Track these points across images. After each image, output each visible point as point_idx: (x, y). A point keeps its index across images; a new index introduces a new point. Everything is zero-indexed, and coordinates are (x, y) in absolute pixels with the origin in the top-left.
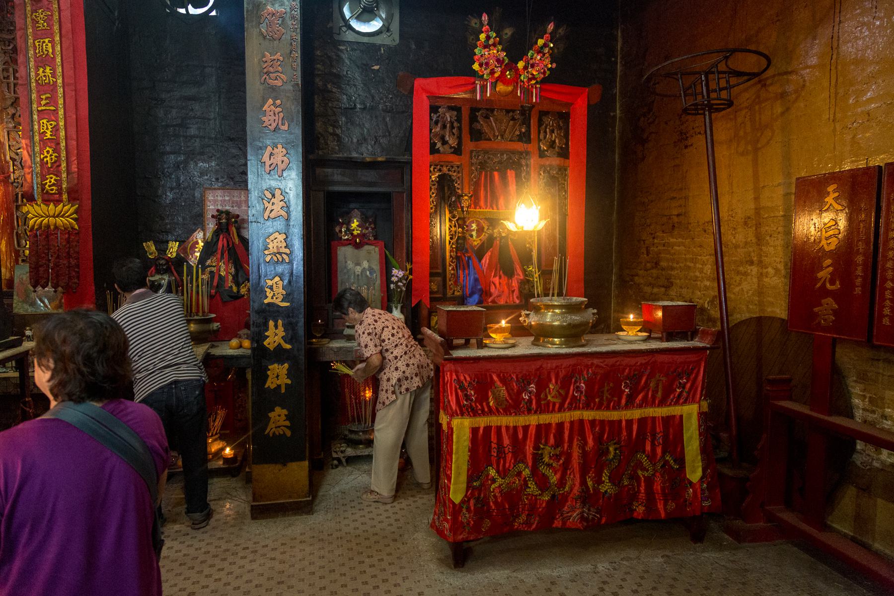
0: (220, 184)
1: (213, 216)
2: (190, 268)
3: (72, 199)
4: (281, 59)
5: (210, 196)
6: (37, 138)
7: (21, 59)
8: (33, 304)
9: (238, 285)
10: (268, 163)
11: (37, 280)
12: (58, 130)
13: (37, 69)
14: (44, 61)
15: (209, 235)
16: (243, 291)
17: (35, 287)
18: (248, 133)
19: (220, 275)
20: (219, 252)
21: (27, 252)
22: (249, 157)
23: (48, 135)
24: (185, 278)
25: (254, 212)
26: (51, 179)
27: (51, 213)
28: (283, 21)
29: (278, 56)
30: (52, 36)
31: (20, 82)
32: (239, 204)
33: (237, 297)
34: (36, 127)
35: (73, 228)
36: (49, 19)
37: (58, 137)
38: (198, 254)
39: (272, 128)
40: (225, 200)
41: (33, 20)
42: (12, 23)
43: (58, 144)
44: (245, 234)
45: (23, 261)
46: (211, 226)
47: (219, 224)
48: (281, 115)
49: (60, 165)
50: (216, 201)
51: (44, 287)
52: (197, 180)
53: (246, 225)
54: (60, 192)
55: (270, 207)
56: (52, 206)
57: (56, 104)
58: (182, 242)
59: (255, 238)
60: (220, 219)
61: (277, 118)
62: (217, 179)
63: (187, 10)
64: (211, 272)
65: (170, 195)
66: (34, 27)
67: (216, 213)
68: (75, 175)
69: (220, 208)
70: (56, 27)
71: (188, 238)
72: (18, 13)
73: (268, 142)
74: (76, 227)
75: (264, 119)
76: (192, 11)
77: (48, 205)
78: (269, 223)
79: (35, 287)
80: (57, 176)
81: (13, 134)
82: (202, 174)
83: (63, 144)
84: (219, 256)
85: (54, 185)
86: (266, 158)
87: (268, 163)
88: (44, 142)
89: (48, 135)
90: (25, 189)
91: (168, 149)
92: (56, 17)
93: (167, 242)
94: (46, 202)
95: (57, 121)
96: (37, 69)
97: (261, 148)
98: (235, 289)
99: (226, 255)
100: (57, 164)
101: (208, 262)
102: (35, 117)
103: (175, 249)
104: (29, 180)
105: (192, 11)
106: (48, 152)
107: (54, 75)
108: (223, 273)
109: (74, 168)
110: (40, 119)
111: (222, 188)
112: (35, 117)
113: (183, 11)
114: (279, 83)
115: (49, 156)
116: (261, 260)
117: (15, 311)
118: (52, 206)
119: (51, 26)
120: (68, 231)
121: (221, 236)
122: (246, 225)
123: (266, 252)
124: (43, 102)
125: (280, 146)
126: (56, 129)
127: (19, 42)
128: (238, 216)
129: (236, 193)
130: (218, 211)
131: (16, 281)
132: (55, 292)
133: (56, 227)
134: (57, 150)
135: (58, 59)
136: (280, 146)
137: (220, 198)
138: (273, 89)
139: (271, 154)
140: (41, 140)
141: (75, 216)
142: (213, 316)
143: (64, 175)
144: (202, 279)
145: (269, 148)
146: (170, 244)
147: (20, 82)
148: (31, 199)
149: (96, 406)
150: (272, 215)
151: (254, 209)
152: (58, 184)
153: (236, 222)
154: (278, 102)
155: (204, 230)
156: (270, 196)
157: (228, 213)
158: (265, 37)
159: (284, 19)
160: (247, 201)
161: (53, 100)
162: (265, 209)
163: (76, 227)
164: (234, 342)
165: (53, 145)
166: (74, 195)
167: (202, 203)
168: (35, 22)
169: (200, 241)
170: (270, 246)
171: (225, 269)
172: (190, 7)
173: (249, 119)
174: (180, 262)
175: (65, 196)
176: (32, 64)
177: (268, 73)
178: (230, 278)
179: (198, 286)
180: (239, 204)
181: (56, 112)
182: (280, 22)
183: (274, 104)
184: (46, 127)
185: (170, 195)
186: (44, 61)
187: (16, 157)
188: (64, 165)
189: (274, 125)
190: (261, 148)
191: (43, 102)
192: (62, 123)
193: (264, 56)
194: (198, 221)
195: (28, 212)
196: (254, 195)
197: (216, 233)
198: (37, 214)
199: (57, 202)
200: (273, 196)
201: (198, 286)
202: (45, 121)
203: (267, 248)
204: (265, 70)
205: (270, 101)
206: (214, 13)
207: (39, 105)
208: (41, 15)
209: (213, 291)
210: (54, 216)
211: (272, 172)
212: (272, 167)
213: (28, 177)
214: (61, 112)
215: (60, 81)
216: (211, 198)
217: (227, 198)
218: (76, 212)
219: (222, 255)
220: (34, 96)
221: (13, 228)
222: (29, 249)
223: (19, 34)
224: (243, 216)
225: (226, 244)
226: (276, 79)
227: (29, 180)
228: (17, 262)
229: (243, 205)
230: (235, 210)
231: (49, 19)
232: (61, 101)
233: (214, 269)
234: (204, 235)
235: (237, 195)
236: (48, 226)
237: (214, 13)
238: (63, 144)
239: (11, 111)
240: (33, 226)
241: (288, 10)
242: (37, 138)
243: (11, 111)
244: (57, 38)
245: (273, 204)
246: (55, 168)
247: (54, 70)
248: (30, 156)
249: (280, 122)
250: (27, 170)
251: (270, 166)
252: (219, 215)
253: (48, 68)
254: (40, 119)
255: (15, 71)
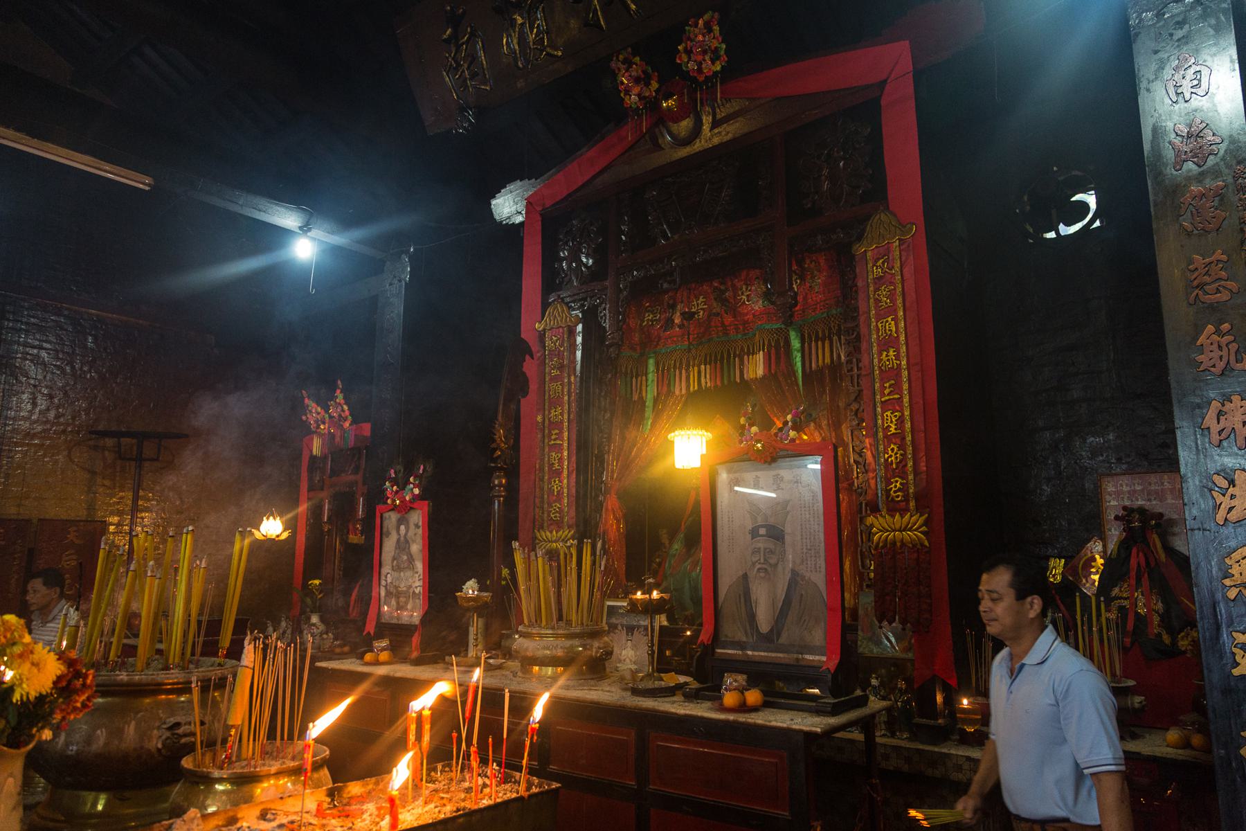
0: (1124, 467)
1: (1117, 518)
2: (1084, 597)
3: (919, 509)
4: (1224, 257)
5: (1109, 486)
6: (881, 434)
7: (864, 346)
8: (879, 643)
9: (1173, 633)
10: (1215, 428)
11: (884, 614)
12: (903, 422)
13: (880, 354)
14: (889, 342)
15: (1112, 546)
16: (1183, 644)
17: (880, 622)
18: (1173, 384)
19: (1137, 614)
20: (1133, 574)
21: (872, 575)
22: (1177, 423)
23: (893, 430)
24: (1078, 617)
25: (1195, 512)
26: (897, 483)
27: (897, 527)
28: (1222, 200)
29: (1219, 255)
30: (895, 312)
31: (863, 373)
32: (1160, 496)
33: (1172, 652)
34: (880, 422)
35: (922, 545)
36: (892, 296)
37: (903, 431)
38: (1096, 577)
39: (1217, 370)
40: (1135, 491)
41: (876, 300)
42: (856, 309)
43: (904, 438)
44: (1179, 545)
45: (868, 586)
46: (1115, 533)
47: (1129, 530)
48: (1234, 347)
49: (906, 465)
50: (1119, 493)
51: (890, 623)
52: (1087, 463)
53: (1176, 530)
54: (906, 499)
55: (1226, 502)
56: (897, 516)
57: (901, 394)
58: (1068, 559)
59: (1201, 556)
60: (1129, 522)
61: (1224, 353)
62: (1119, 460)
63: (1057, 233)
64: (1122, 609)
65: (1047, 489)
66: (877, 307)
67: (1121, 513)
68: (924, 476)
69: (1127, 503)
70: (899, 301)
71: (1079, 552)
72: (861, 296)
73: (1212, 394)
74: (926, 543)
75: (1200, 358)
76: (1066, 230)
77: (893, 516)
78: (1230, 530)
79: (880, 622)
80: (902, 478)
81: (856, 433)
82: (1095, 453)
83: (909, 438)
84: (1133, 582)
85: (899, 490)
86: (1210, 419)
87: (1215, 428)
88: (888, 439)
89: (893, 430)
90: (869, 497)
91: (1041, 423)
92: (899, 289)
93: (1047, 558)
94: (892, 511)
95: (902, 411)
96: (880, 354)
97: (1199, 406)
98: (1166, 639)
99: (1145, 580)
100: (902, 463)
101: (1116, 591)
102: (879, 409)
103: (1059, 570)
104: (873, 486)
105: (1066, 230)
106: (893, 450)
107: (898, 357)
108: (1142, 611)
109: (923, 466)
110: (884, 411)
111: (1129, 472)
112: (879, 409)
113: (1052, 235)
114: (1224, 296)
115: (892, 454)
116: (1219, 596)
117: (860, 650)
118: (897, 516)
119: (893, 301)
120: (916, 547)
121: (1134, 551)
122: (1176, 530)
123: (1227, 582)
124: (886, 392)
125: (1236, 398)
126: (901, 421)
127: (863, 330)
128: (1161, 515)
129: (1153, 478)
130: (1125, 508)
131: (861, 612)
132: (904, 629)
133: (903, 544)
134: (902, 447)
135: (902, 338)
136: (1236, 398)
137: (1125, 489)
138: (1213, 308)
139: (1220, 414)
140: (886, 436)
141: (924, 528)
142: (1131, 683)
143: (911, 477)
144: (1107, 619)
145: (1215, 405)
146: (1052, 563)
147: (863, 373)
148: (875, 509)
149: (843, 426)
150: (1233, 516)
151: (1197, 505)
152: (904, 489)
153: (1158, 525)
154: (1226, 326)
155: (1103, 539)
156: (1225, 484)
157: (1142, 511)
158: (1189, 234)
159: (1222, 198)
160: (1180, 493)
161: (897, 388)
162: (1217, 507)
163: (926, 543)
164: (1173, 735)
165: (898, 441)
166: (923, 502)
167: (1097, 498)
168: (877, 301)
169: (1097, 557)
170: (1235, 571)
171: (1144, 603)
172: (1062, 227)
173: (1171, 363)
174: (1070, 588)
175: (912, 504)
176: (875, 349)
177: (1201, 286)
178: (1156, 619)
179: (1101, 630)
180: (1160, 496)
181: (900, 399)
182: (1216, 203)
183: (1218, 332)
184: (889, 420)
185: (1047, 489)
186: (889, 342)
187: (860, 460)
188: (910, 464)
189: (1222, 364)
190: (1199, 406)
191: (886, 392)
192: (907, 413)
193: (1191, 262)
194: (1094, 526)
195: (872, 526)
196: (1192, 485)
197: (1125, 545)
198: (882, 528)
199: (903, 512)
200: (1232, 483)
201: (1101, 630)
202: (889, 413)
203: (1227, 575)
204: (1195, 283)
205: (1210, 328)
206: (1097, 224)
207: (883, 395)
208: (884, 291)
209: (1128, 640)
210: (900, 530)
211: (1225, 444)
212: (1224, 435)
213: (872, 482)
214: (906, 400)
215: (904, 362)
216: (1111, 489)
217: (1139, 488)
218: (926, 523)
219: (1139, 579)
220: (877, 385)
221: (857, 545)
222: (874, 571)
223: (862, 319)
224: (1171, 514)
225: (1143, 563)
226: (1218, 291)
227: (873, 486)
228: (861, 587)
229: (1169, 497)
230: (1155, 506)
231: (892, 296)
232: (905, 386)
233: (1126, 603)
234: (1105, 546)
235: (1157, 481)
236: (894, 543)
237: (1097, 224)
238: (909, 438)
239: (855, 406)
240: (878, 544)
241: (1230, 180)
242: (881, 434)
243: (855, 406)
244: (901, 313)
245: (1233, 497)
246: (901, 471)
247: (898, 351)
248: (874, 457)
249: (1232, 358)
250: (871, 475)
251: (1220, 433)
252: (1127, 515)
253: (891, 350)
254: (884, 411)
255: (859, 361)
